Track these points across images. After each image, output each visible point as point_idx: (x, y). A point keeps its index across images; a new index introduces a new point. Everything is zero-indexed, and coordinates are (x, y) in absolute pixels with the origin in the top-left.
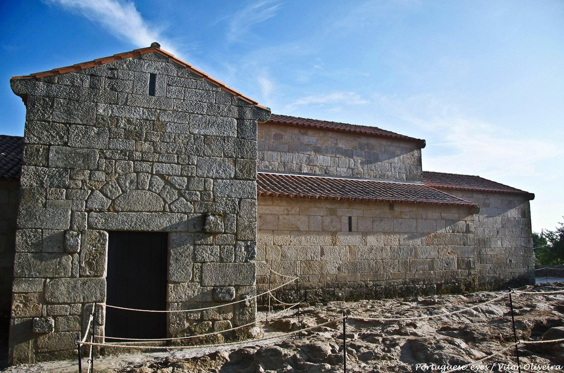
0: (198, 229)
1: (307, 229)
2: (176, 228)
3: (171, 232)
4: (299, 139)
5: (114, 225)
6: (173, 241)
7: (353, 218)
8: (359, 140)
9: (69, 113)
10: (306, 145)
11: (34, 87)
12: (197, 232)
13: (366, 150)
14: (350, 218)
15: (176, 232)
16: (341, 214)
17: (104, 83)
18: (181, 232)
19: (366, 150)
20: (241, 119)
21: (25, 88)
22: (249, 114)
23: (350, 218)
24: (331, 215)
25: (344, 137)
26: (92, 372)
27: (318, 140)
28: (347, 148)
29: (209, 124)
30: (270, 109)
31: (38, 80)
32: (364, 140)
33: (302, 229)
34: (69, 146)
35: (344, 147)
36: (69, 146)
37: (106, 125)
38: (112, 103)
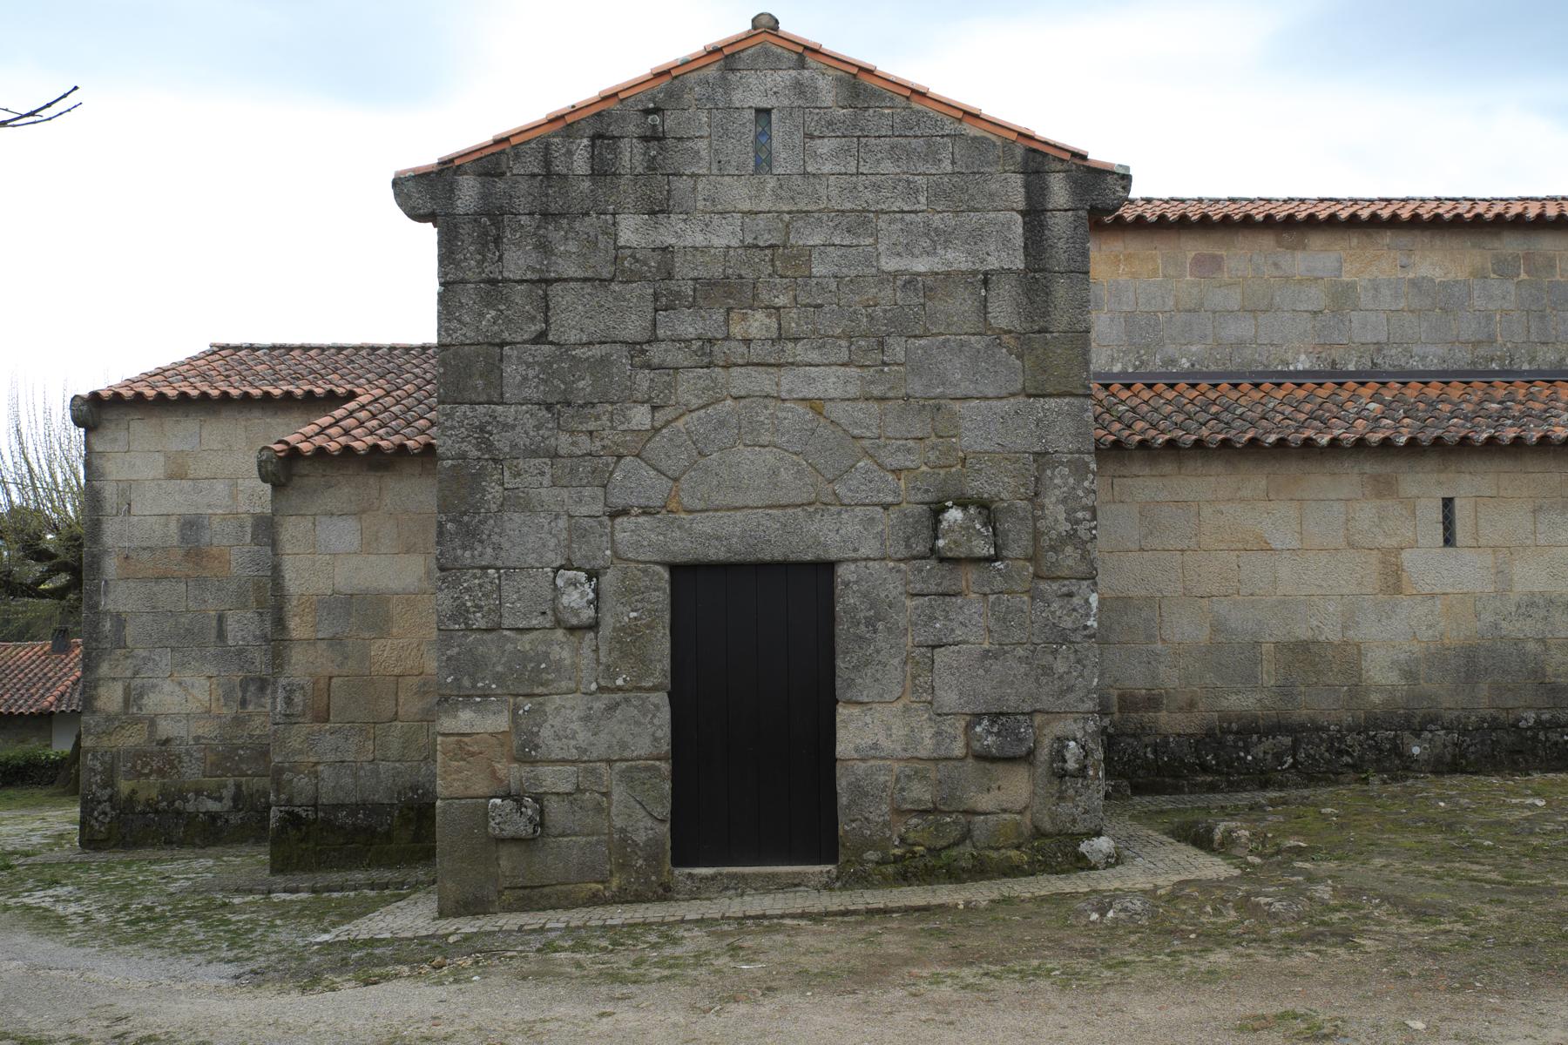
0: (920, 547)
1: (1295, 544)
2: (856, 550)
3: (840, 561)
4: (1276, 265)
5: (685, 548)
6: (847, 584)
7: (1457, 502)
8: (1497, 244)
9: (544, 247)
10: (1300, 282)
11: (451, 190)
12: (915, 558)
13: (1523, 276)
14: (1448, 503)
15: (855, 560)
16: (1415, 491)
17: (631, 155)
18: (867, 559)
19: (1523, 276)
20: (1034, 214)
21: (423, 193)
22: (1059, 192)
23: (1448, 503)
24: (1379, 495)
25: (1438, 243)
26: (3, 124)
27: (1340, 261)
28: (1451, 276)
29: (943, 238)
30: (1127, 168)
31: (459, 170)
32: (1511, 245)
33: (1277, 545)
34: (551, 343)
35: (1438, 274)
36: (551, 343)
37: (659, 275)
38: (657, 210)
